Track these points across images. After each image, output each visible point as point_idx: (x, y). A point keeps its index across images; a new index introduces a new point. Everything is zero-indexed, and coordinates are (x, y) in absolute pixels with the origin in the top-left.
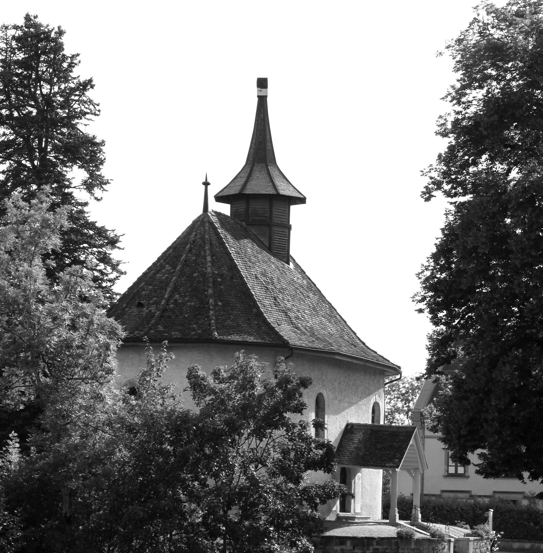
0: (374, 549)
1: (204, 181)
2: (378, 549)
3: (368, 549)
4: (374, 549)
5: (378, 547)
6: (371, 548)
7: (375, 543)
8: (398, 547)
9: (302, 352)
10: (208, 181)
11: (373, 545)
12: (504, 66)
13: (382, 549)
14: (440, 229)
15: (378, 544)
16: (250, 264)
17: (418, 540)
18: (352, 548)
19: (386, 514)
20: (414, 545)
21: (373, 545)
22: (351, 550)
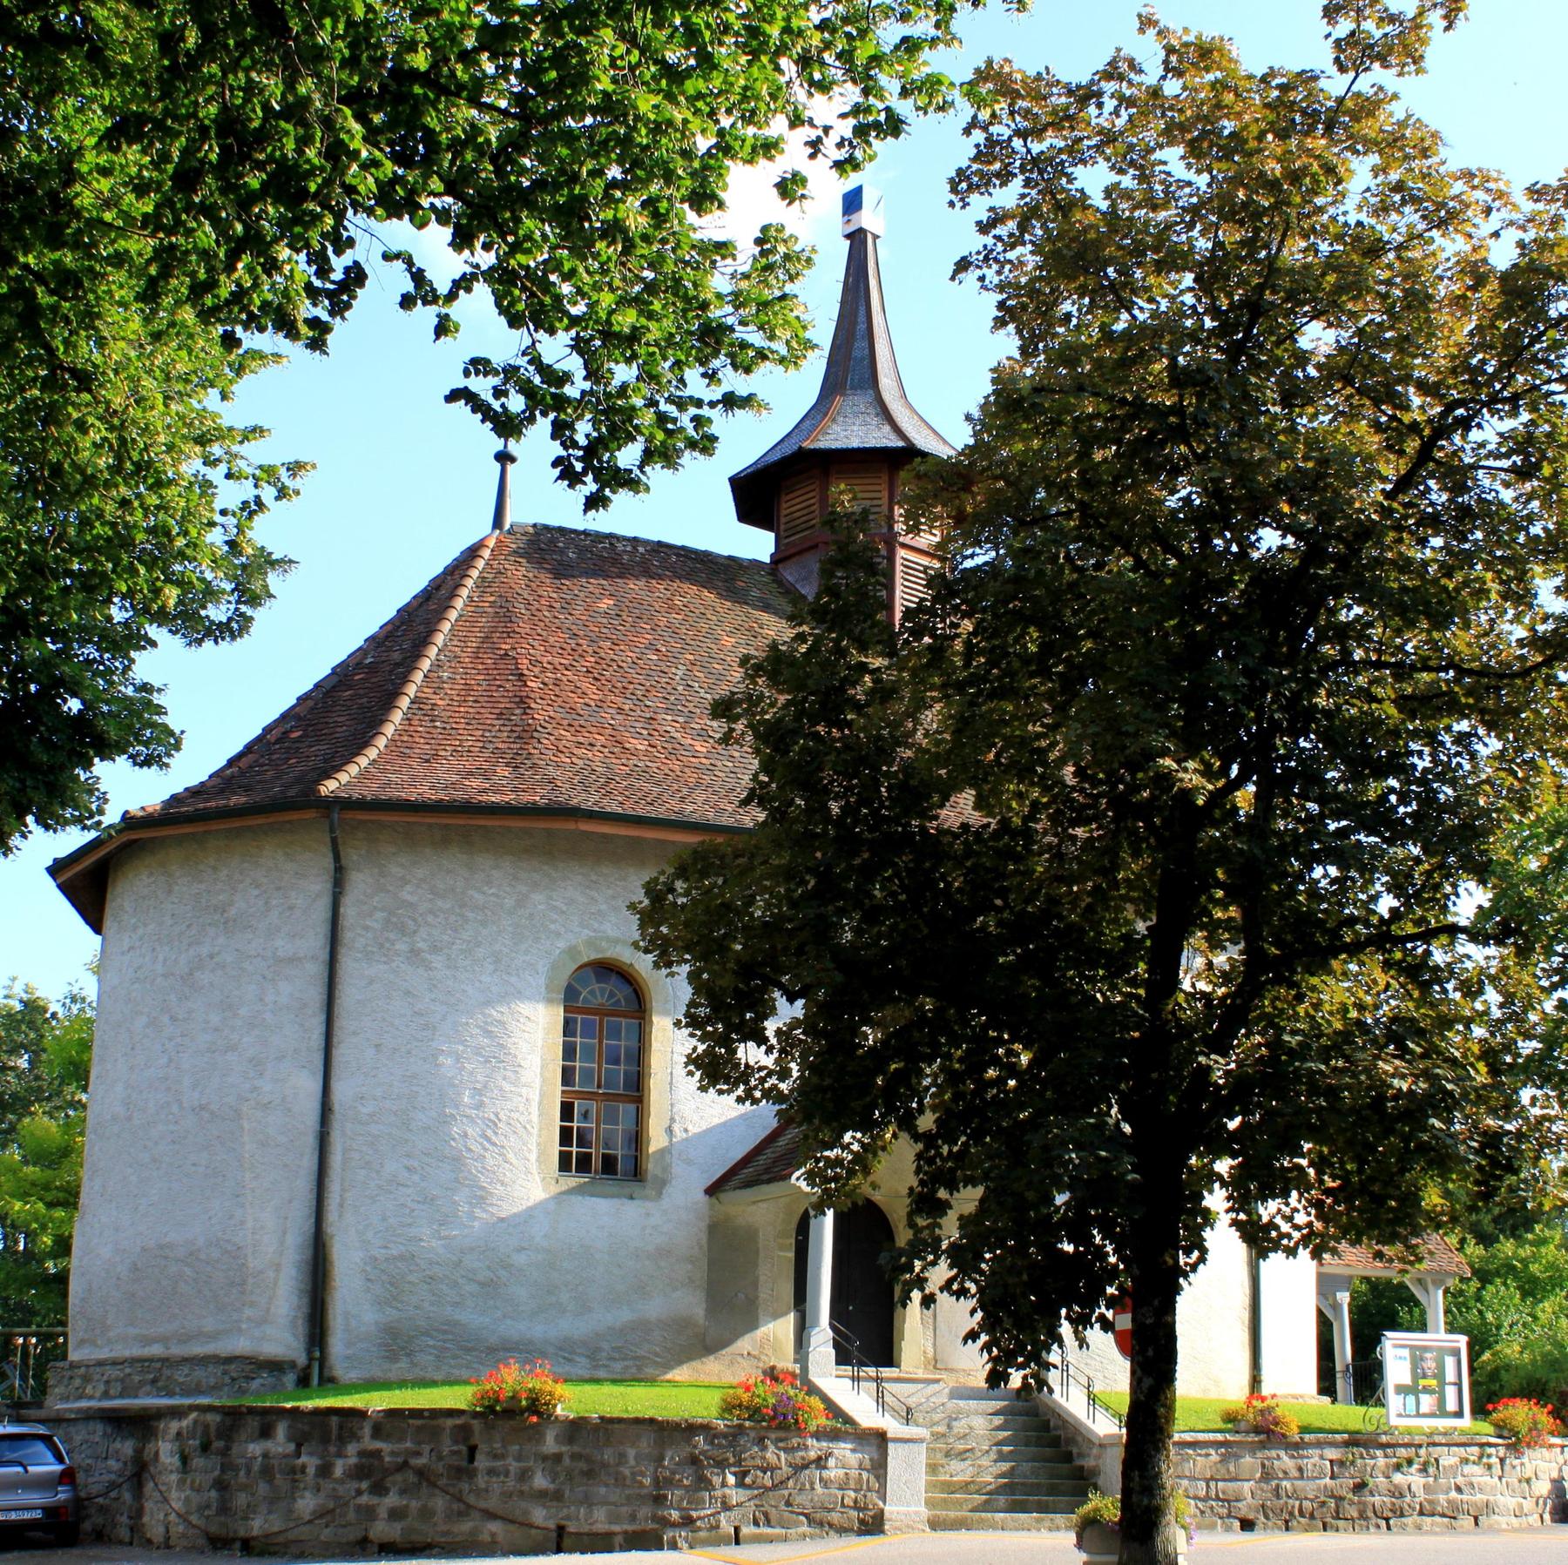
0: (362, 1454)
1: (510, 468)
2: (377, 1454)
3: (340, 1455)
4: (362, 1454)
5: (378, 1445)
6: (352, 1449)
7: (367, 1431)
8: (472, 1450)
9: (172, 832)
10: (498, 466)
11: (359, 1439)
12: (566, 191)
13: (393, 1453)
14: (585, 511)
15: (377, 1432)
16: (1492, 637)
17: (577, 1428)
18: (292, 1447)
19: (1327, 1385)
20: (557, 1439)
21: (359, 1439)
22: (286, 1456)
